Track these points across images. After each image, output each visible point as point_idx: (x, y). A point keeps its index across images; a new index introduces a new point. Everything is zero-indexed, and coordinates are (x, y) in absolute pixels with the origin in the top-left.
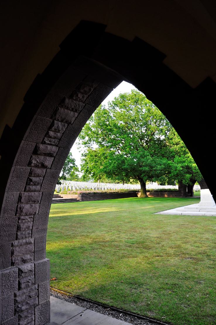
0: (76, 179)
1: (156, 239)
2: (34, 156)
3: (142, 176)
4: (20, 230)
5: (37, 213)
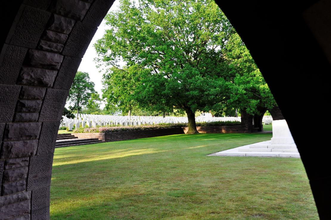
0: (97, 112)
1: (210, 189)
2: (25, 69)
3: (189, 103)
4: (7, 180)
5: (35, 153)
